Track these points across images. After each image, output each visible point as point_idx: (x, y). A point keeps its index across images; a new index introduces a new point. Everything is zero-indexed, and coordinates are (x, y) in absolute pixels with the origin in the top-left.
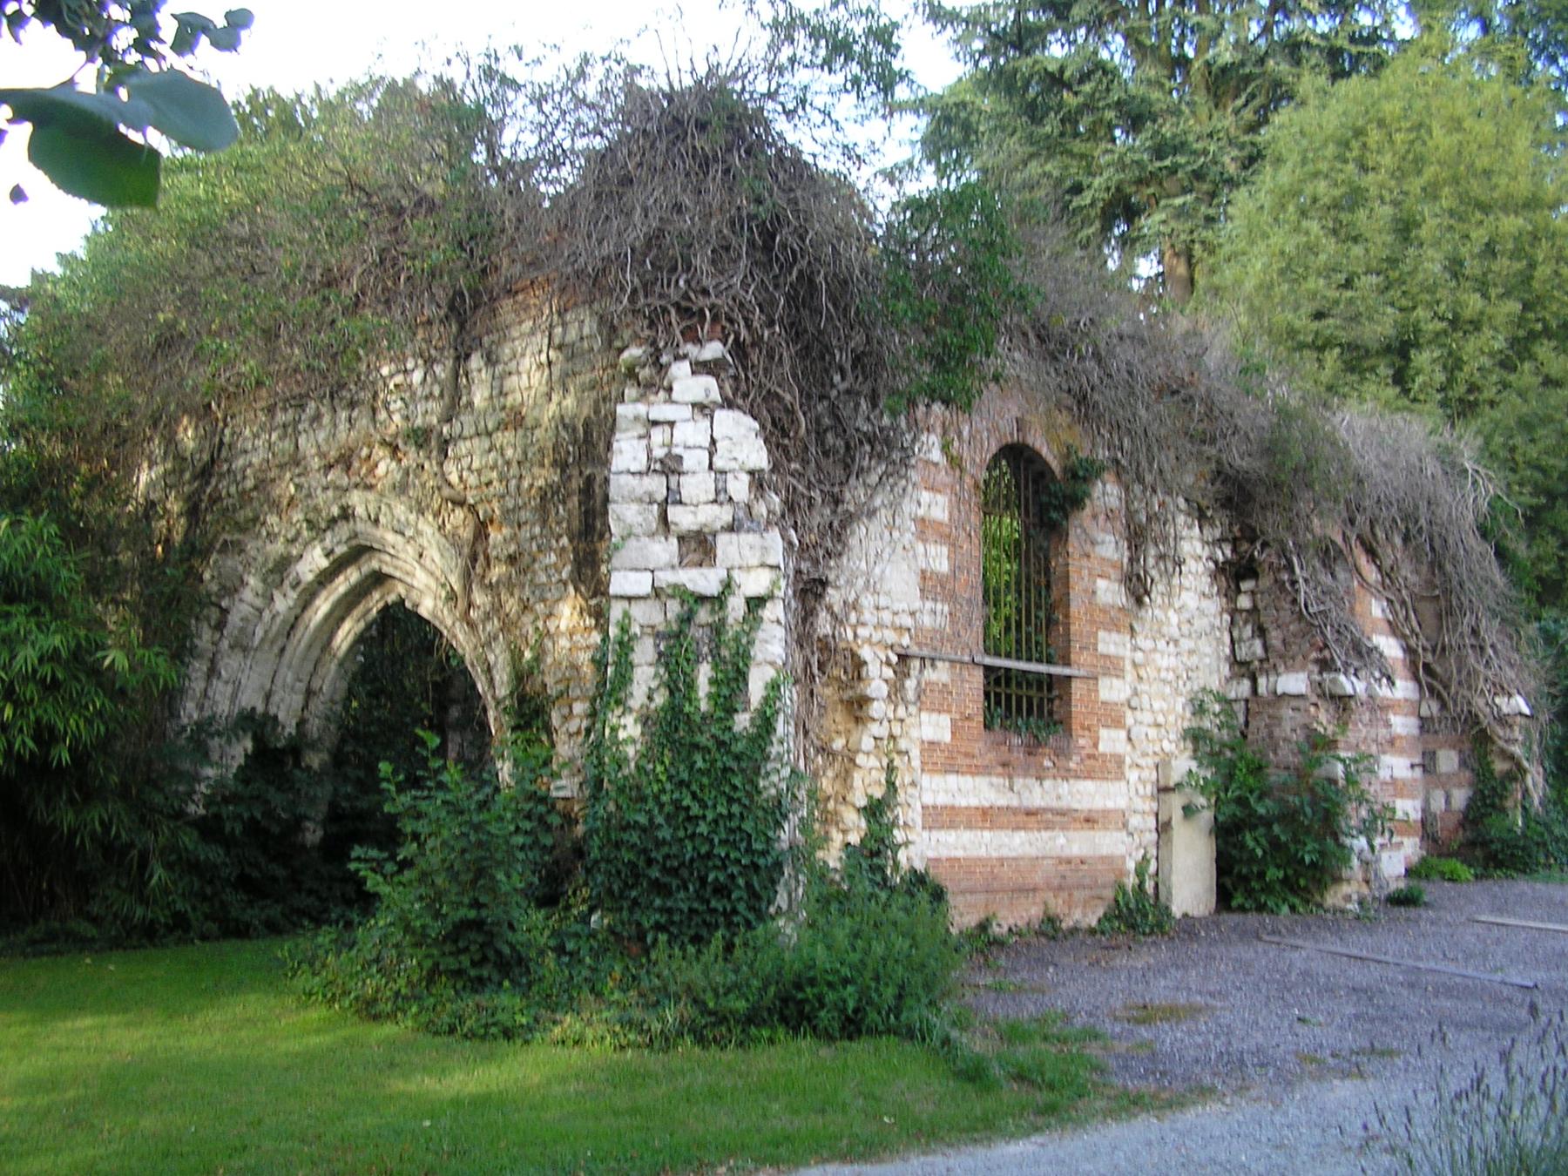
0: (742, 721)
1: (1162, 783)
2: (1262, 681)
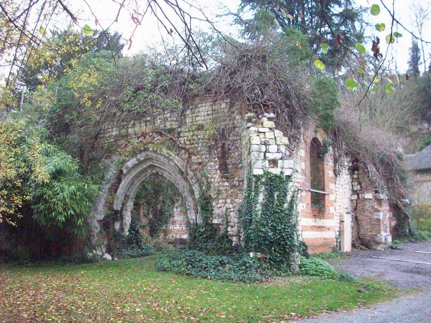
0: (286, 206)
1: (341, 220)
2: (360, 195)
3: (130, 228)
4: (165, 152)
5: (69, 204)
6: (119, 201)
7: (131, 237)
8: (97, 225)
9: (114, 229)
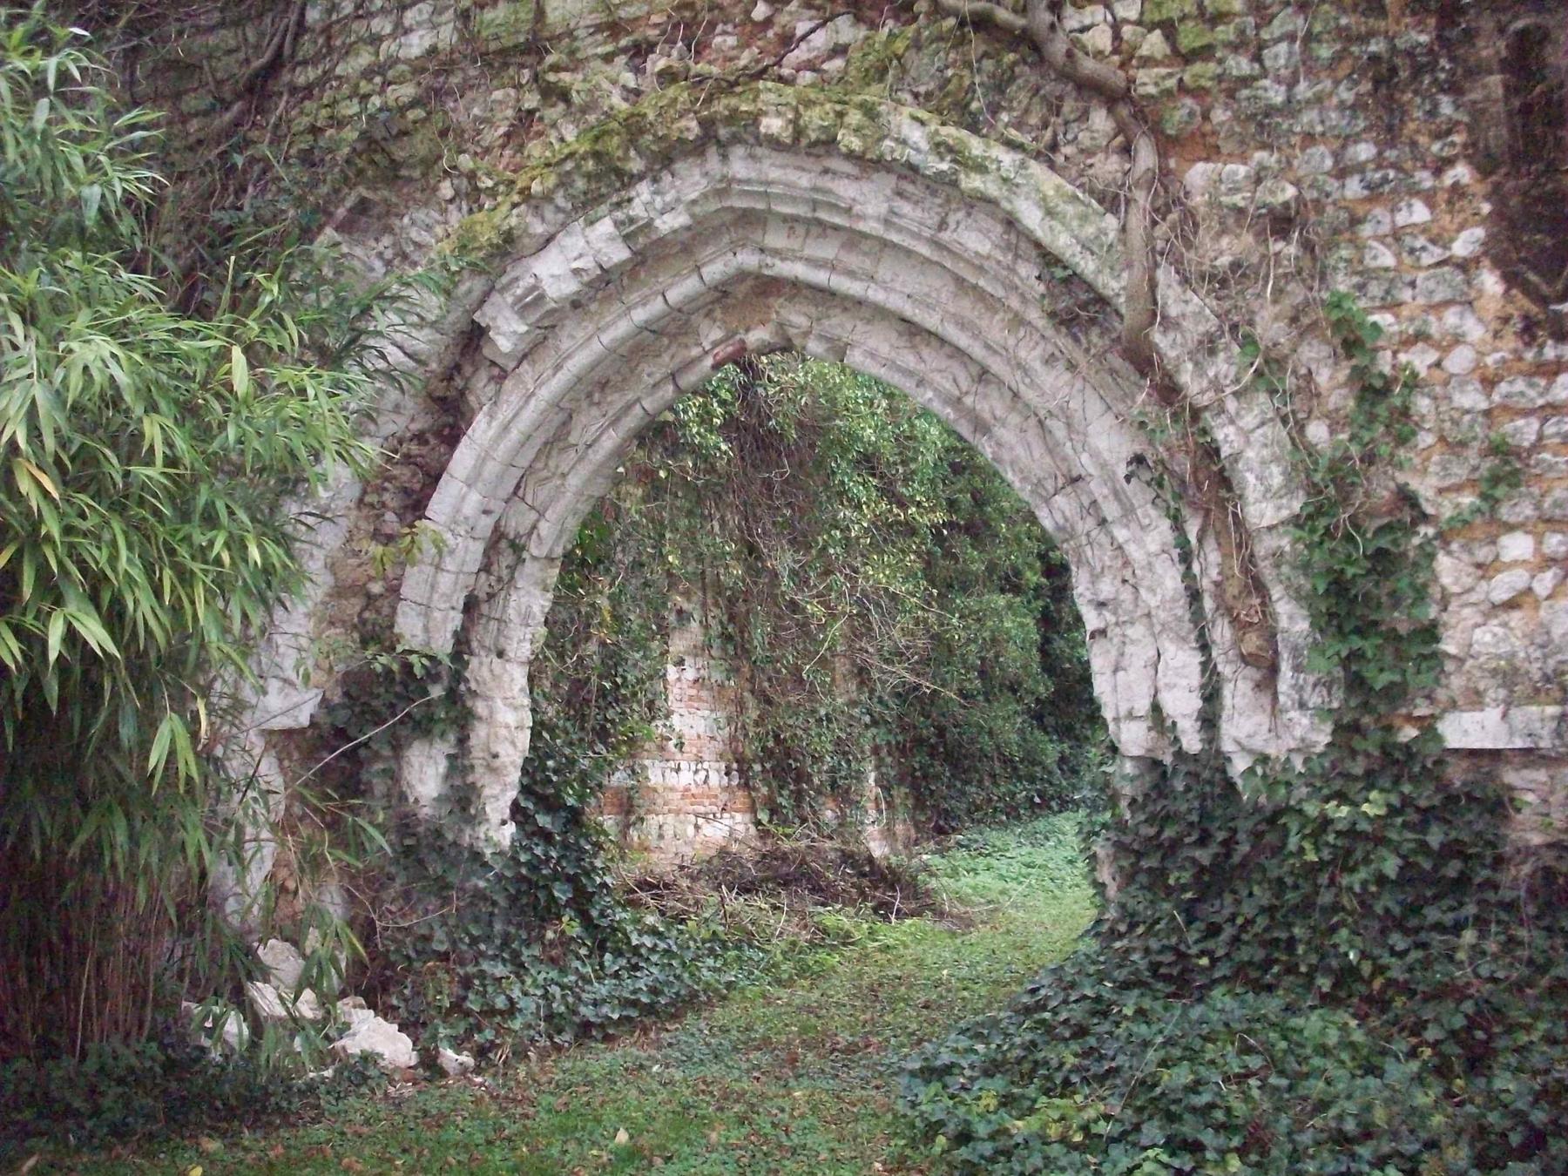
3: (525, 790)
4: (916, 135)
5: (52, 527)
6: (445, 581)
7: (534, 866)
8: (271, 774)
9: (398, 796)
